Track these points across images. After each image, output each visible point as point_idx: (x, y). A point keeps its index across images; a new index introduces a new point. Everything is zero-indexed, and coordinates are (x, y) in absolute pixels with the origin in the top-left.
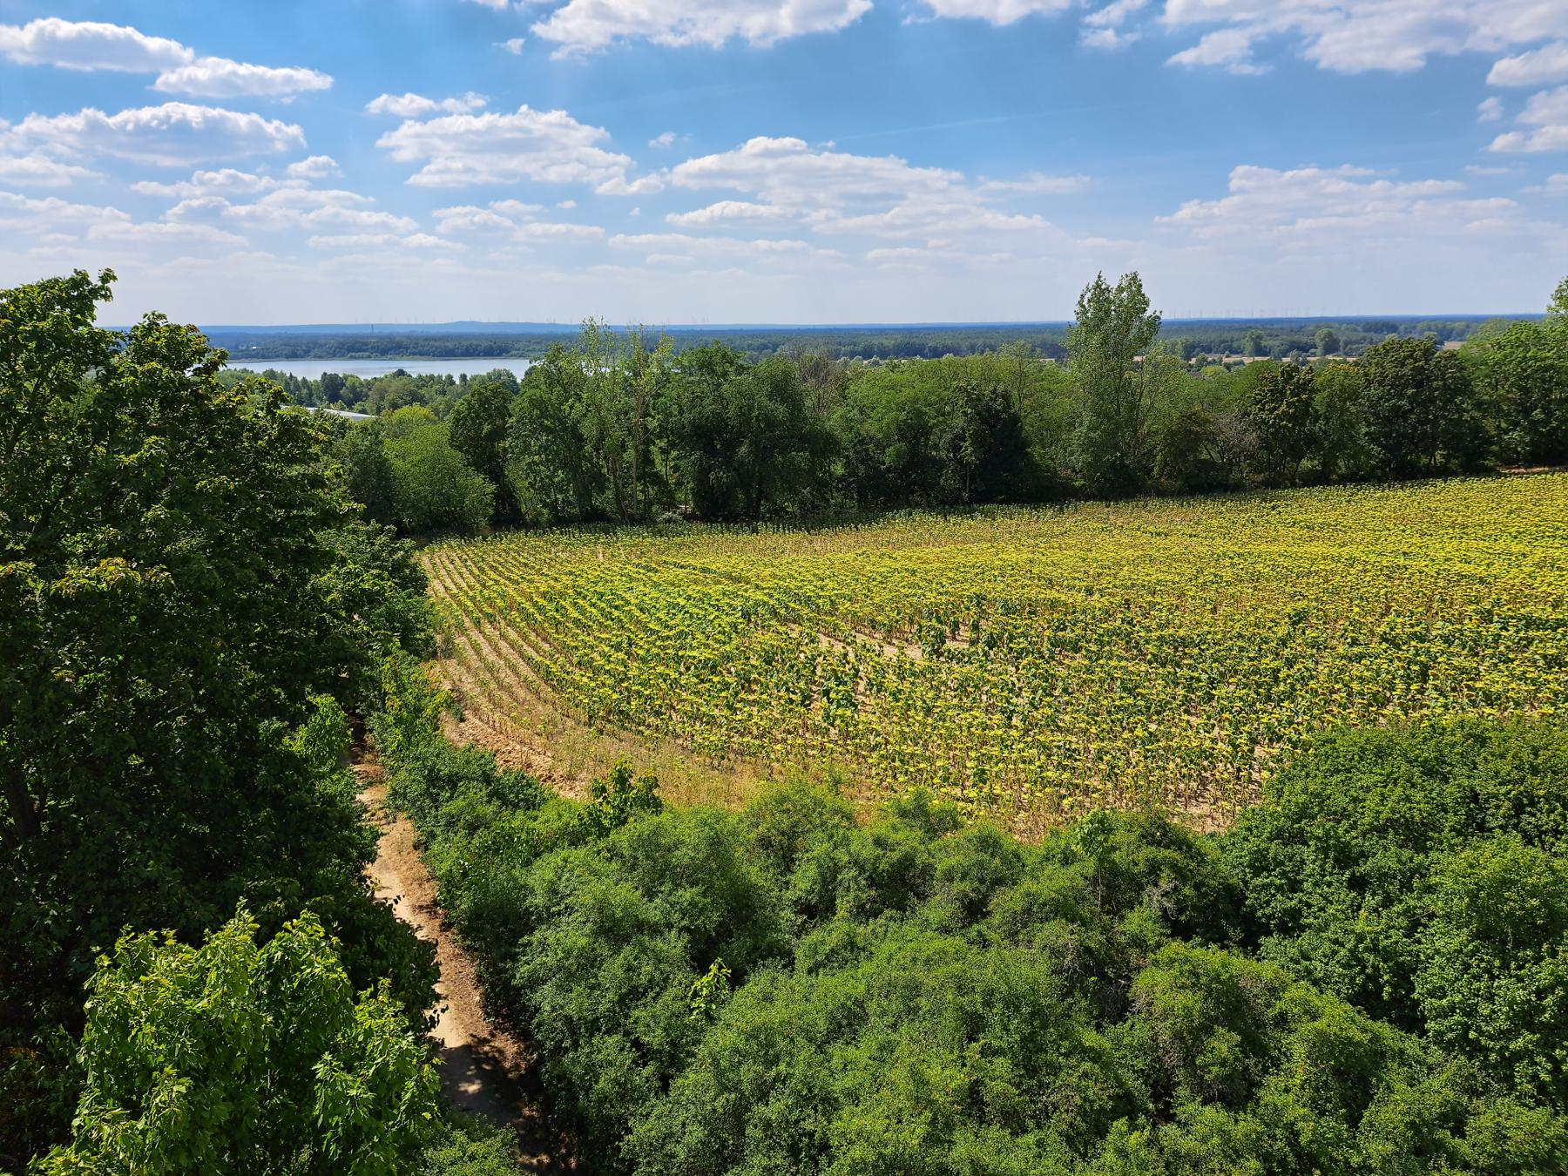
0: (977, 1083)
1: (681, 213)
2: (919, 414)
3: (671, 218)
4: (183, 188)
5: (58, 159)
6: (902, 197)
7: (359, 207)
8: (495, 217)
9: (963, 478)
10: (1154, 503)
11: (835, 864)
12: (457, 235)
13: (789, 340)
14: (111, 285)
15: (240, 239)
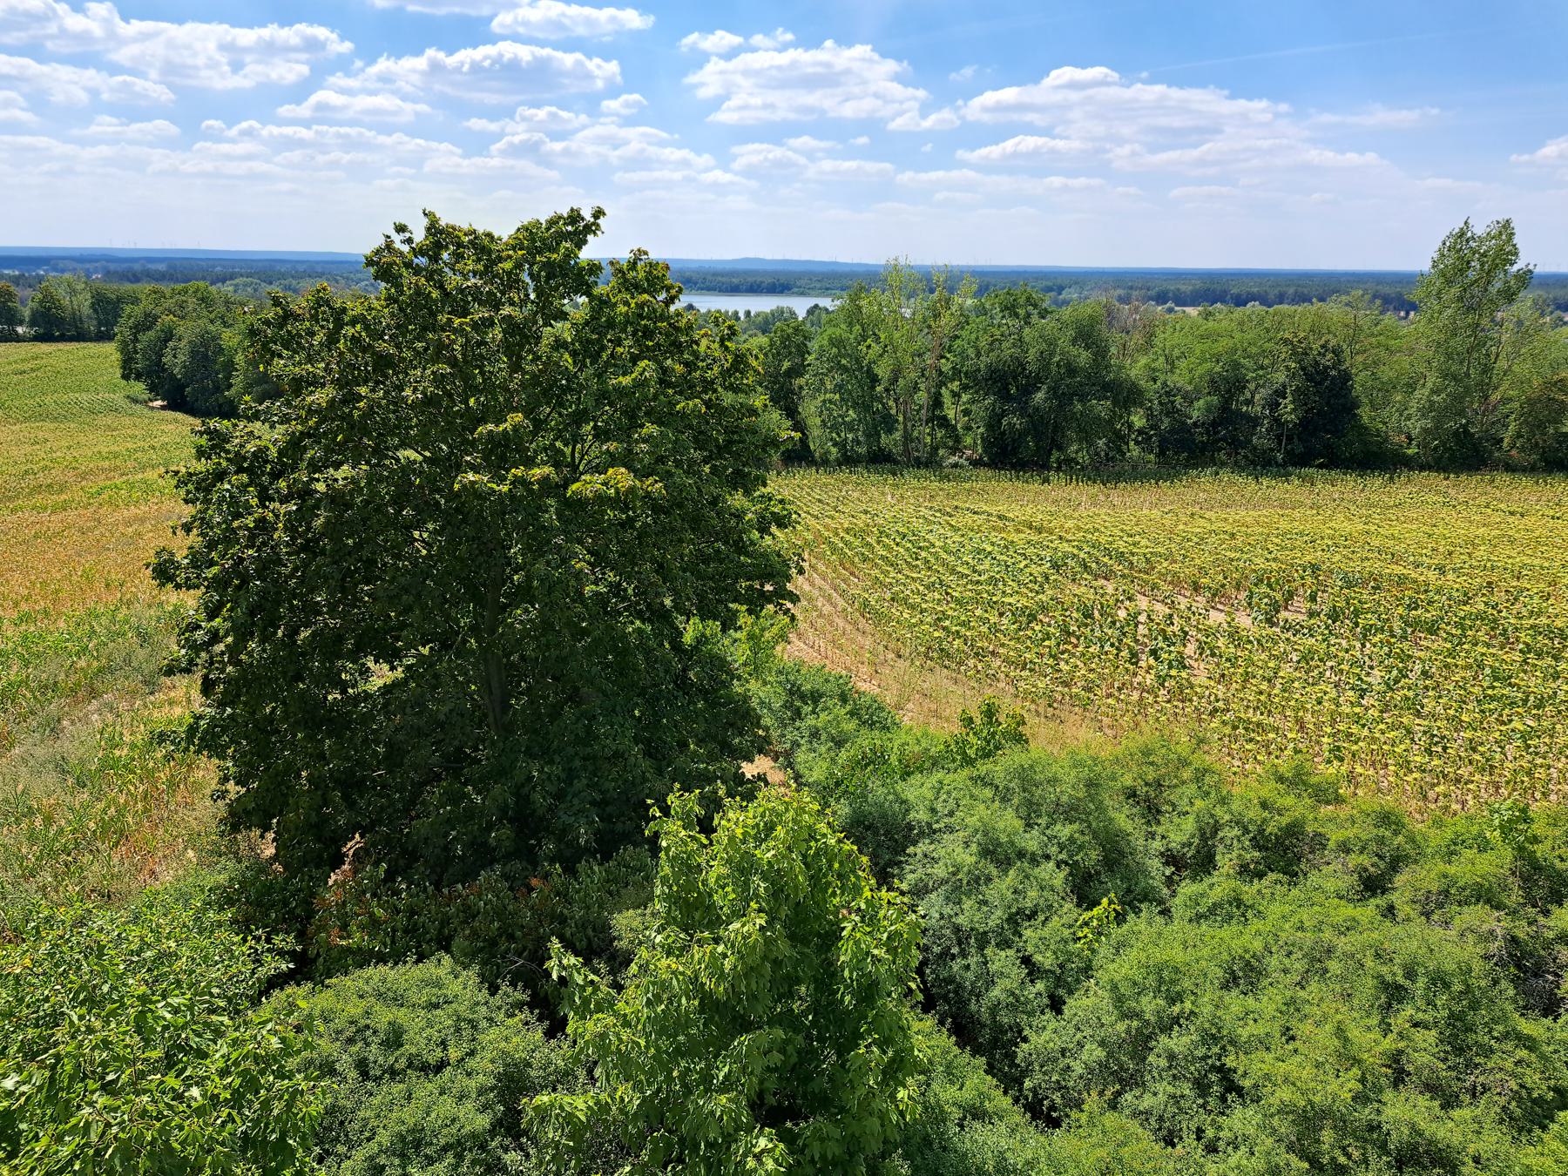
0: (1400, 1052)
1: (973, 150)
2: (1236, 366)
3: (961, 154)
4: (510, 126)
5: (404, 99)
6: (1217, 131)
7: (662, 144)
8: (790, 154)
9: (1279, 437)
10: (1503, 478)
11: (1217, 821)
12: (750, 172)
13: (1076, 283)
14: (601, 221)
15: (553, 174)
